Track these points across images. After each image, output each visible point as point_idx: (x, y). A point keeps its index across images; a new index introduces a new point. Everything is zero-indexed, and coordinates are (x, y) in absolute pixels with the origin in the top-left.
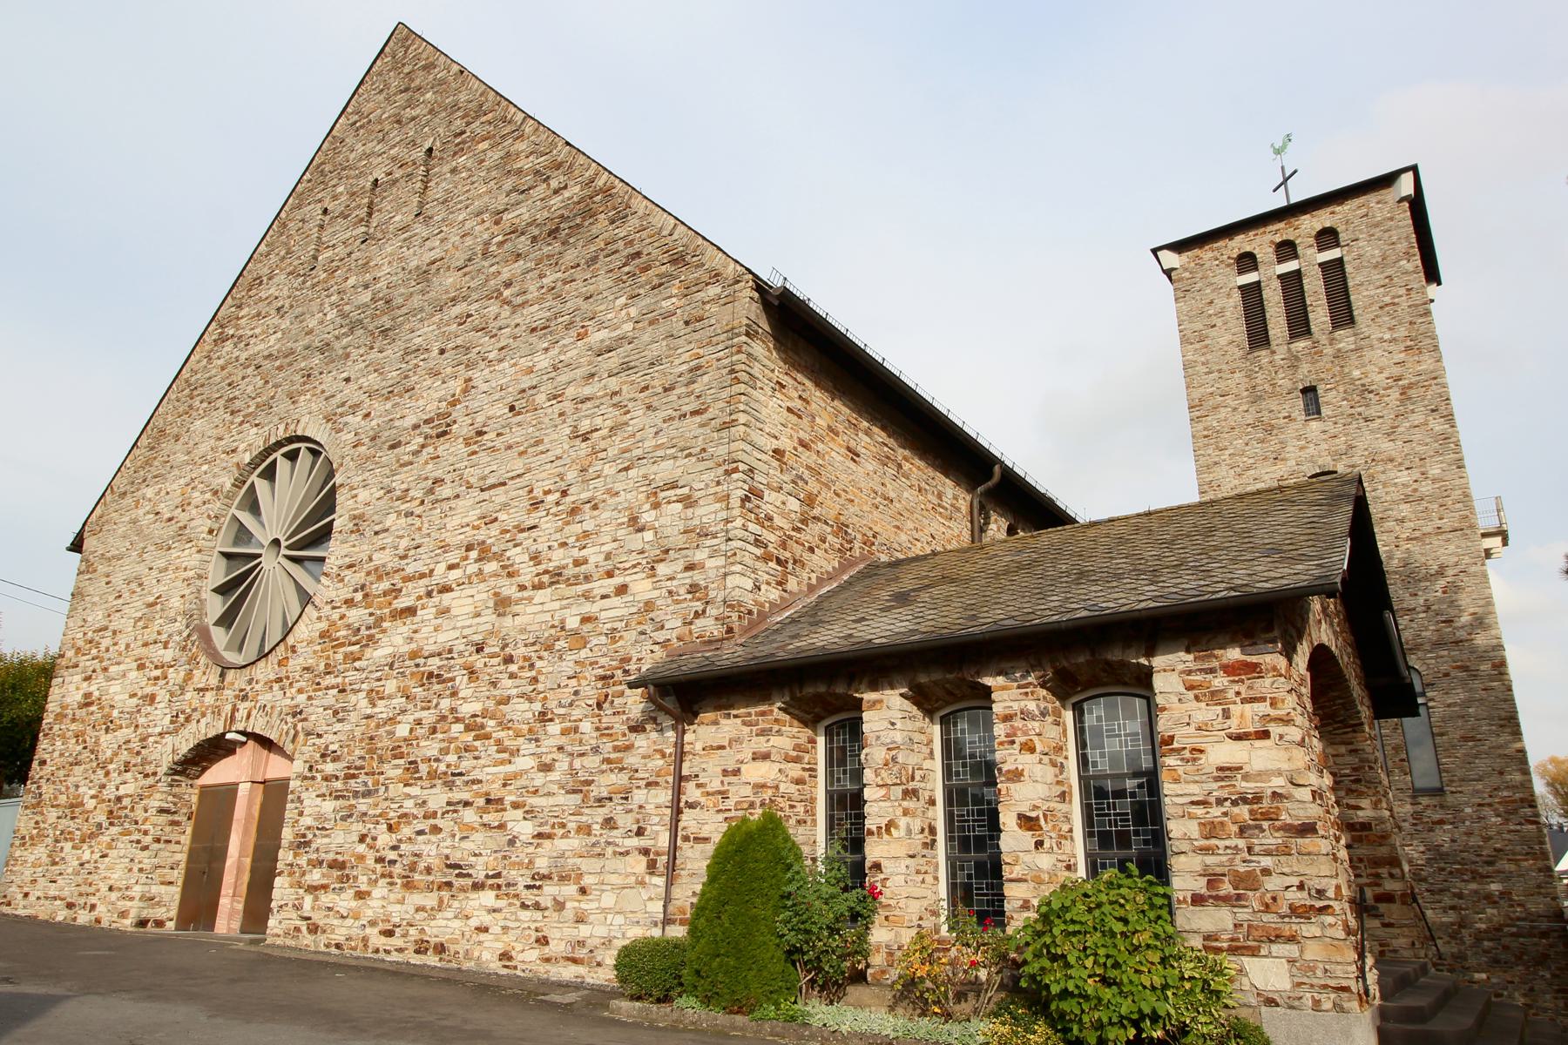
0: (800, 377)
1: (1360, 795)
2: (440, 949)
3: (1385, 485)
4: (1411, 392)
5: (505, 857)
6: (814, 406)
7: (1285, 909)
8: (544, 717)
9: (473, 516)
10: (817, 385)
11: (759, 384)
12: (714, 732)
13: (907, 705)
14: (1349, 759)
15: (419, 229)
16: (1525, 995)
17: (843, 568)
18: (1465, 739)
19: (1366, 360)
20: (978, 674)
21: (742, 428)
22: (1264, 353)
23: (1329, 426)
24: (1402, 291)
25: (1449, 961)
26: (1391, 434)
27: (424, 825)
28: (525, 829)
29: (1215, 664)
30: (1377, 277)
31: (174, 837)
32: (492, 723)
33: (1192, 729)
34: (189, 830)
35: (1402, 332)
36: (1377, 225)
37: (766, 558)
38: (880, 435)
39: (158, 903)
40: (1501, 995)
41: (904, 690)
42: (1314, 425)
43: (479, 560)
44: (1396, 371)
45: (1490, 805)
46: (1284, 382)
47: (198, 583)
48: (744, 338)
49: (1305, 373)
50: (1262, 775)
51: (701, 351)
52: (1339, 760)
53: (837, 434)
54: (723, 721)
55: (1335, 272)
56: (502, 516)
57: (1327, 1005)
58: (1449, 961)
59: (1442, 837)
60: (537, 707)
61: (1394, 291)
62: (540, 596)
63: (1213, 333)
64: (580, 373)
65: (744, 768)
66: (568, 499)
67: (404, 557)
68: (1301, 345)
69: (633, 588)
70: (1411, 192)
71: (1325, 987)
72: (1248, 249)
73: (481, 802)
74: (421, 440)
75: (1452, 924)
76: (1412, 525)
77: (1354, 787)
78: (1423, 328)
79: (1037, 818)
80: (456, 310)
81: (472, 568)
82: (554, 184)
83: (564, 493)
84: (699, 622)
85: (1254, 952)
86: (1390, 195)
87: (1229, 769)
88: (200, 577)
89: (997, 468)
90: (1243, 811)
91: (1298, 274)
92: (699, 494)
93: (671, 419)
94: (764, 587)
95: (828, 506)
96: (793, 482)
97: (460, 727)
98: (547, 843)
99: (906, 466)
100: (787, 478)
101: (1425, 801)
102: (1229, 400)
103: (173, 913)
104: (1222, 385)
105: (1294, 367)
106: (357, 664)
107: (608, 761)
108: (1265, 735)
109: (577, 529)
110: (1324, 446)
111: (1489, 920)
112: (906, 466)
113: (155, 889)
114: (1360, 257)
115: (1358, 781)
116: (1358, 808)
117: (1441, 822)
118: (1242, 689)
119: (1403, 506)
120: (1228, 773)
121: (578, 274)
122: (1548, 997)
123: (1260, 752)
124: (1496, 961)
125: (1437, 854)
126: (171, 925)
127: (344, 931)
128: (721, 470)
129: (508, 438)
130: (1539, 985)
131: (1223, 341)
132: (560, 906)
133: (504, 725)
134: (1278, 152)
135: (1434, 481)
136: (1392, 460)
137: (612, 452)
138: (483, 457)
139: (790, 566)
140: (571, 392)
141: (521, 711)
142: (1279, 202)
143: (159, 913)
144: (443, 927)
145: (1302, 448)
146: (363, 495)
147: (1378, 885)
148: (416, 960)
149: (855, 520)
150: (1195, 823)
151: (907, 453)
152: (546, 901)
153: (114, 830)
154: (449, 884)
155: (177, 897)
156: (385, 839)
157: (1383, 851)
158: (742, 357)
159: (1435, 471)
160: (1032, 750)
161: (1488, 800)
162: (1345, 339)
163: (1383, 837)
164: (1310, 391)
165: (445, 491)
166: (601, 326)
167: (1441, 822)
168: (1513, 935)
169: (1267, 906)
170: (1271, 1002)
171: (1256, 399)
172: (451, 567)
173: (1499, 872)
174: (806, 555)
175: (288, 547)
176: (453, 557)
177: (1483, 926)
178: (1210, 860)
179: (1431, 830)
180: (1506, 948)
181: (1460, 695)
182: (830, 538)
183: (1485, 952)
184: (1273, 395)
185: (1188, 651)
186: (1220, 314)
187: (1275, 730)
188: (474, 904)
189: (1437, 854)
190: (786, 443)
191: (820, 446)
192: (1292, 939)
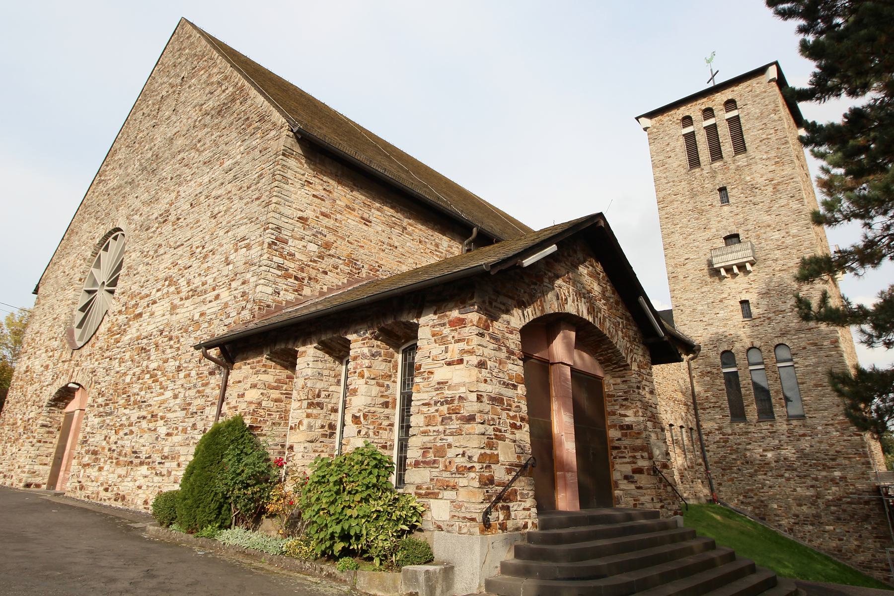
0: (325, 178)
1: (627, 408)
2: (123, 498)
3: (766, 240)
4: (780, 187)
5: (154, 447)
6: (335, 194)
7: (454, 469)
8: (179, 369)
9: (168, 264)
10: (339, 183)
11: (290, 181)
12: (242, 371)
13: (320, 353)
14: (622, 386)
15: (174, 118)
16: (856, 540)
17: (350, 283)
18: (816, 386)
19: (753, 170)
20: (346, 333)
21: (274, 205)
22: (697, 170)
23: (734, 208)
24: (772, 131)
25: (811, 518)
26: (768, 211)
27: (126, 430)
28: (162, 431)
29: (446, 320)
30: (758, 124)
31: (49, 440)
32: (160, 373)
33: (430, 360)
34: (58, 436)
35: (773, 154)
36: (757, 96)
37: (287, 276)
38: (388, 211)
39: (38, 475)
40: (842, 540)
41: (315, 345)
42: (726, 208)
43: (168, 286)
44: (770, 176)
45: (832, 425)
46: (709, 186)
47: (72, 306)
48: (281, 157)
49: (720, 181)
50: (457, 386)
51: (263, 166)
52: (616, 387)
53: (354, 210)
54: (243, 367)
55: (734, 123)
56: (180, 262)
57: (465, 530)
58: (811, 518)
59: (805, 444)
60: (177, 363)
61: (768, 131)
62: (187, 303)
63: (669, 160)
64: (218, 183)
65: (246, 392)
66: (205, 250)
67: (142, 287)
68: (717, 164)
69: (222, 296)
70: (776, 76)
71: (464, 518)
72: (687, 114)
73: (149, 416)
74: (157, 225)
75: (812, 496)
76: (782, 262)
77: (624, 403)
78: (784, 151)
79: (359, 417)
80: (180, 157)
81: (165, 291)
82: (224, 87)
83: (203, 247)
84: (243, 313)
85: (435, 496)
86: (764, 79)
87: (442, 383)
88: (73, 303)
89: (475, 230)
90: (444, 409)
91: (714, 126)
92: (253, 242)
93: (248, 203)
94: (282, 293)
95: (342, 248)
96: (314, 235)
97: (148, 376)
98: (170, 438)
99: (410, 229)
100: (308, 233)
101: (795, 422)
102: (679, 197)
103: (46, 481)
104: (675, 189)
105: (714, 177)
106: (119, 344)
107: (198, 392)
108: (461, 361)
109: (205, 265)
110: (731, 220)
111: (834, 494)
112: (410, 229)
113: (36, 467)
114: (748, 114)
115: (626, 399)
116: (626, 416)
117: (804, 435)
118: (455, 334)
119: (777, 252)
120: (441, 386)
121: (225, 132)
122: (870, 540)
123: (458, 372)
124: (839, 519)
125: (802, 454)
126: (44, 487)
127: (91, 489)
128: (262, 229)
129: (188, 221)
130: (865, 534)
131: (675, 165)
132: (169, 473)
133: (164, 375)
134: (708, 62)
135: (794, 236)
136: (769, 226)
137: (224, 223)
138: (178, 231)
139: (306, 281)
140: (214, 194)
141: (172, 365)
142: (711, 85)
143: (38, 480)
144: (127, 487)
145: (719, 222)
146: (133, 255)
147: (635, 463)
148: (114, 504)
149: (364, 257)
150: (422, 416)
151: (411, 221)
152: (165, 472)
153: (25, 436)
154: (131, 462)
155: (49, 472)
156: (113, 438)
157: (638, 442)
158: (279, 167)
159: (794, 231)
160: (363, 377)
161: (831, 422)
162: (742, 159)
163: (638, 433)
164: (722, 190)
165: (161, 251)
166: (230, 158)
167: (804, 435)
168: (848, 503)
169: (446, 467)
170: (440, 528)
171: (693, 196)
172: (158, 290)
173: (838, 465)
174: (320, 276)
175: (108, 286)
176: (159, 286)
177: (831, 498)
178: (426, 439)
179: (798, 440)
180: (844, 511)
181: (813, 360)
182: (341, 266)
183: (832, 513)
184: (703, 193)
185: (435, 313)
186: (673, 150)
187: (466, 358)
188: (139, 473)
189: (802, 454)
190: (309, 213)
191: (339, 216)
192: (454, 488)
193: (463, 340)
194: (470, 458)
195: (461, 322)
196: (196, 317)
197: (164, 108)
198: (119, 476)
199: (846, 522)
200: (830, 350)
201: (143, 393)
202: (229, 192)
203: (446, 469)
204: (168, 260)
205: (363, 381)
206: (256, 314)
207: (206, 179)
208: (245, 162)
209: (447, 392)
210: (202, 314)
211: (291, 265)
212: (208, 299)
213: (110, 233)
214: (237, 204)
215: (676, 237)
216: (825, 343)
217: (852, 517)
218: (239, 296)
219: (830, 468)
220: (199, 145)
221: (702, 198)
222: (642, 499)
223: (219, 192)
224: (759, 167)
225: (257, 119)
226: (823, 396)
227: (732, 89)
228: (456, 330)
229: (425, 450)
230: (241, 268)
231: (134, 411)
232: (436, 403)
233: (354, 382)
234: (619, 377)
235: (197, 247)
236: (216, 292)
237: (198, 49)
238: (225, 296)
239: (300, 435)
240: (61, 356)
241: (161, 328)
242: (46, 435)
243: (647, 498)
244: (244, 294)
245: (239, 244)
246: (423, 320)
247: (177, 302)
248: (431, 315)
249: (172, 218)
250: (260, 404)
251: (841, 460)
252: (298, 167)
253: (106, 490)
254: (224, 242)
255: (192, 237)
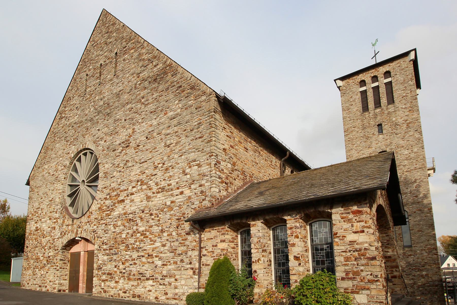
1: (389, 248)
2: (139, 296)
3: (400, 155)
4: (410, 125)
5: (154, 271)
7: (367, 281)
8: (162, 231)
10: (235, 128)
12: (210, 234)
13: (263, 225)
15: (115, 80)
16: (430, 302)
17: (244, 185)
18: (419, 231)
19: (397, 114)
20: (283, 216)
22: (367, 113)
24: (409, 92)
25: (410, 294)
26: (403, 139)
28: (159, 263)
30: (402, 87)
31: (65, 267)
32: (148, 233)
33: (342, 231)
34: (69, 265)
35: (408, 105)
36: (402, 70)
37: (222, 182)
38: (254, 143)
39: (63, 285)
41: (262, 221)
42: (381, 136)
43: (141, 185)
44: (406, 118)
46: (372, 123)
47: (63, 194)
48: (213, 113)
49: (379, 120)
50: (362, 243)
51: (201, 118)
54: (212, 231)
55: (389, 85)
56: (147, 171)
58: (410, 294)
59: (411, 259)
60: (160, 228)
62: (159, 195)
63: (352, 107)
64: (166, 126)
65: (218, 244)
66: (165, 166)
67: (120, 185)
68: (378, 110)
69: (185, 192)
71: (377, 302)
72: (363, 79)
73: (147, 256)
77: (387, 246)
79: (299, 257)
81: (139, 188)
82: (154, 63)
83: (164, 164)
84: (204, 202)
85: (358, 293)
86: (407, 59)
87: (353, 242)
90: (356, 254)
91: (378, 87)
93: (193, 140)
95: (239, 166)
99: (262, 153)
100: (227, 157)
101: (406, 249)
102: (356, 129)
103: (67, 288)
105: (375, 118)
107: (181, 243)
108: (363, 232)
111: (422, 282)
112: (262, 153)
113: (62, 281)
115: (388, 244)
117: (411, 255)
119: (405, 161)
120: (352, 243)
124: (423, 293)
125: (409, 264)
127: (113, 292)
128: (208, 156)
131: (355, 110)
132: (170, 284)
133: (151, 234)
135: (415, 153)
136: (403, 147)
140: (164, 132)
141: (156, 229)
143: (64, 288)
145: (377, 144)
147: (392, 273)
148: (133, 299)
150: (343, 257)
151: (262, 148)
152: (166, 283)
153: (49, 265)
154: (140, 279)
155: (68, 283)
156: (121, 267)
157: (394, 264)
158: (213, 119)
160: (298, 238)
162: (391, 108)
164: (380, 125)
165: (130, 164)
167: (411, 255)
168: (428, 286)
169: (362, 280)
171: (364, 128)
172: (133, 187)
173: (425, 269)
175: (87, 182)
178: (346, 268)
179: (408, 257)
180: (426, 290)
183: (420, 291)
184: (369, 127)
185: (342, 207)
186: (354, 101)
187: (366, 230)
189: (409, 264)
191: (237, 147)
192: (368, 289)
193: (363, 221)
194: (377, 276)
195: (360, 212)
196: (168, 203)
197: (105, 72)
198: (132, 286)
199: (426, 294)
200: (427, 213)
201: (138, 243)
202: (176, 132)
203: (362, 281)
204: (136, 170)
205: (299, 239)
206: (214, 203)
207: (155, 122)
208: (184, 114)
209: (357, 246)
210: (172, 202)
211: (223, 176)
212: (175, 194)
213: (81, 151)
214: (183, 139)
215: (353, 151)
216: (425, 210)
217: (429, 292)
218: (199, 193)
219: (421, 270)
220: (143, 100)
221: (368, 130)
222: (396, 289)
223: (168, 132)
224: (400, 113)
225: (189, 87)
226: (422, 236)
227: (389, 64)
228: (357, 216)
229: (347, 273)
230: (197, 177)
231: (134, 253)
232: (350, 251)
233: (292, 240)
234: (385, 233)
235: (159, 164)
236: (180, 190)
237: (125, 34)
238: (187, 192)
239: (260, 266)
240: (64, 221)
241: (142, 208)
242: (63, 265)
243: (398, 289)
244: (202, 192)
245: (192, 163)
246: (334, 211)
247: (150, 194)
248: (340, 208)
249: (133, 144)
250: (227, 250)
251: (427, 267)
252: (219, 118)
253: (125, 292)
254: (179, 161)
255: (153, 157)
